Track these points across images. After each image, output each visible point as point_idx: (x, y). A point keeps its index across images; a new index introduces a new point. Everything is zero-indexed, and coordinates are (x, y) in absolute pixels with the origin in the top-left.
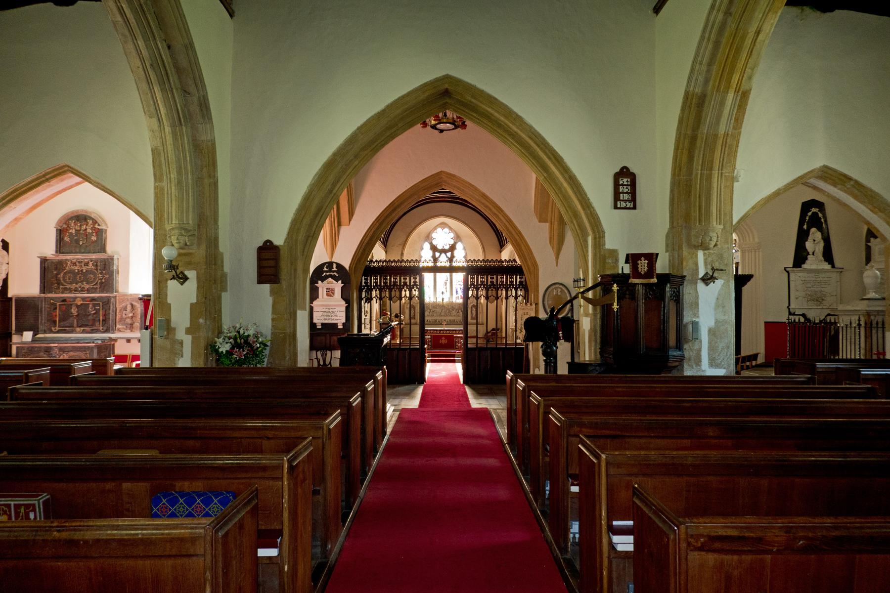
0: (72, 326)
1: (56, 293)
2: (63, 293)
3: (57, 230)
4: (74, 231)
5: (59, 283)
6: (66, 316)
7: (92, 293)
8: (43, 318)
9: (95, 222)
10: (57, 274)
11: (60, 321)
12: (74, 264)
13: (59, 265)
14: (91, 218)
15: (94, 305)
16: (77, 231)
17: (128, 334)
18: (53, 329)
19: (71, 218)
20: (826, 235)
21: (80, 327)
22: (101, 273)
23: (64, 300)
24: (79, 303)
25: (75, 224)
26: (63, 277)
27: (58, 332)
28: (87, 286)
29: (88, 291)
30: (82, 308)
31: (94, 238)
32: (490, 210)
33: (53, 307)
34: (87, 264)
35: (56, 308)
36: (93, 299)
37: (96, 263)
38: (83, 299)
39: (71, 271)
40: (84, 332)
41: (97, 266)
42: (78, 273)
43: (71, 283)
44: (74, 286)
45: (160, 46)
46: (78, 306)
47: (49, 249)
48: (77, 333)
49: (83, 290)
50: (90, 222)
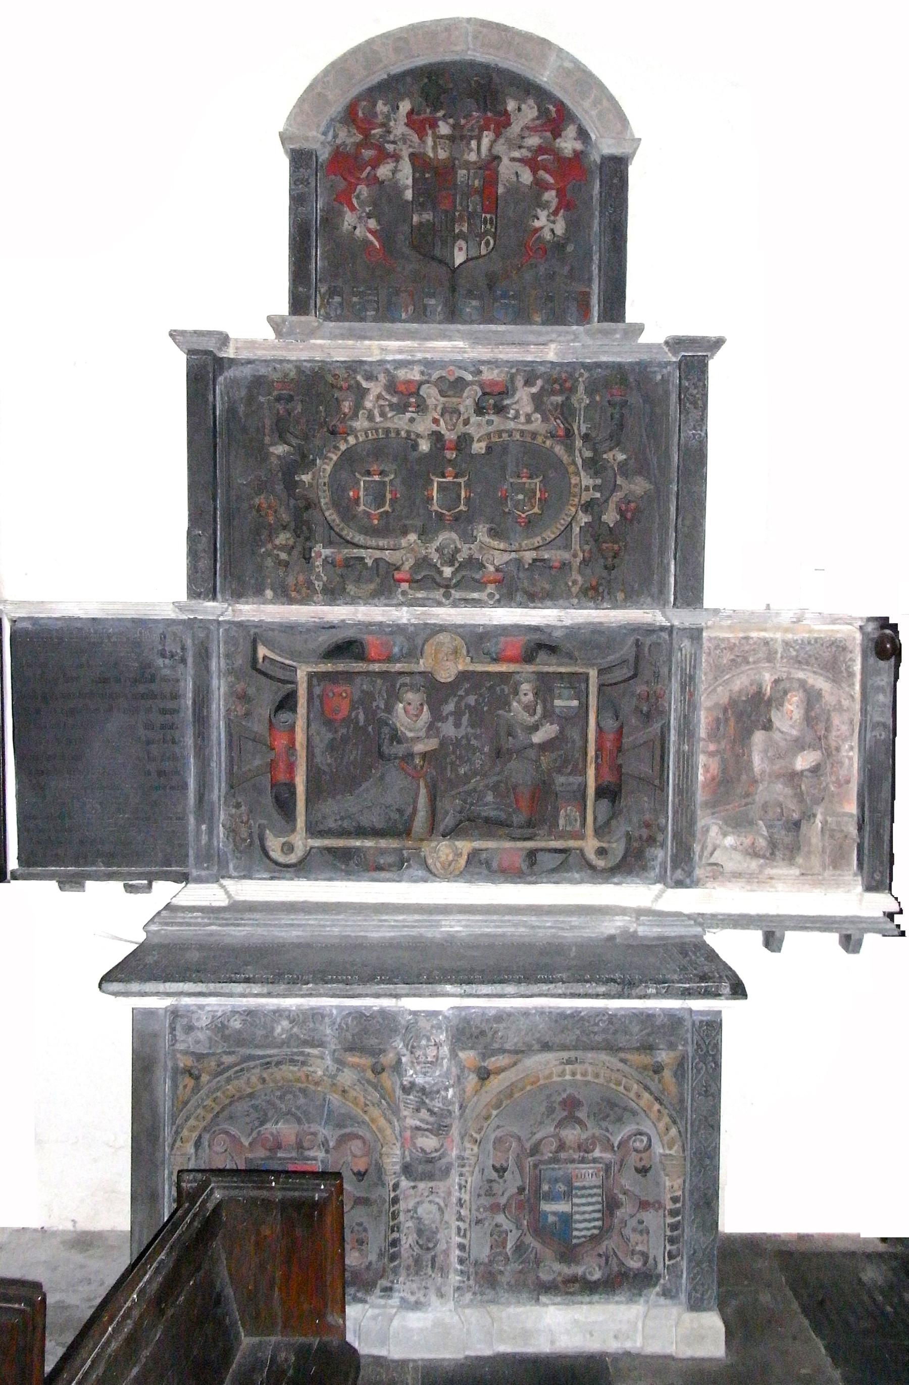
0: (403, 830)
1: (285, 595)
2: (333, 594)
3: (300, 159)
4: (406, 174)
5: (303, 523)
6: (360, 746)
7: (533, 598)
8: (207, 768)
9: (556, 117)
10: (303, 461)
11: (315, 792)
12: (406, 396)
13: (311, 399)
14: (529, 89)
15: (545, 685)
16: (434, 178)
17: (784, 896)
18: (274, 844)
19: (390, 88)
20: (880, 716)
21: (453, 833)
22: (594, 465)
23: (347, 647)
24: (446, 673)
25: (419, 124)
26: (338, 490)
27: (301, 868)
28: (497, 556)
29: (510, 590)
30: (480, 694)
31: (548, 224)
32: (220, 772)
33: (268, 696)
34: (494, 399)
35: (287, 703)
36: (541, 644)
37: (557, 383)
38: (478, 640)
39: (388, 449)
40: (479, 867)
41: (566, 412)
42: (435, 461)
43: (388, 528)
44: (406, 549)
45: (218, 584)
46: (435, 692)
47: (246, 292)
48: (431, 874)
49: (467, 580)
50: (524, 114)
